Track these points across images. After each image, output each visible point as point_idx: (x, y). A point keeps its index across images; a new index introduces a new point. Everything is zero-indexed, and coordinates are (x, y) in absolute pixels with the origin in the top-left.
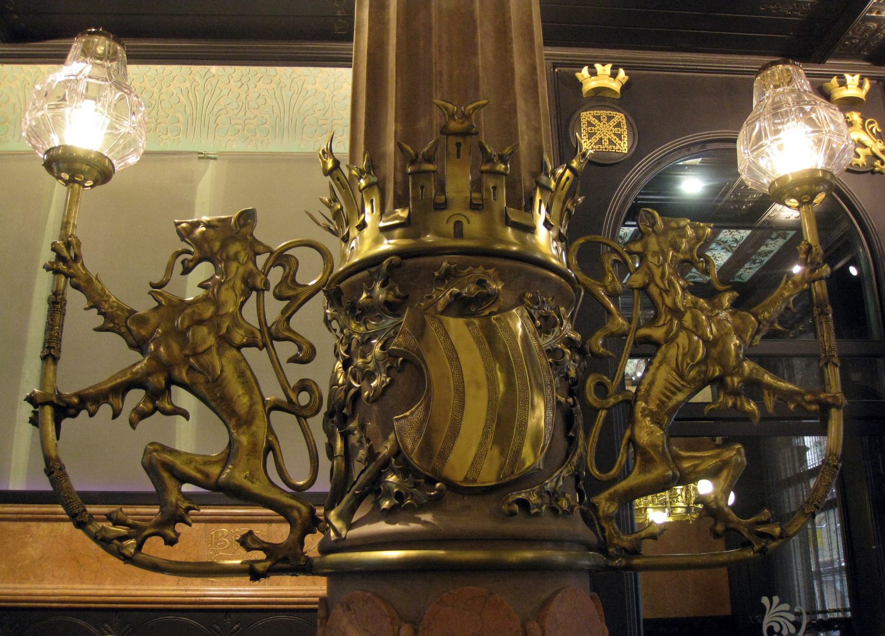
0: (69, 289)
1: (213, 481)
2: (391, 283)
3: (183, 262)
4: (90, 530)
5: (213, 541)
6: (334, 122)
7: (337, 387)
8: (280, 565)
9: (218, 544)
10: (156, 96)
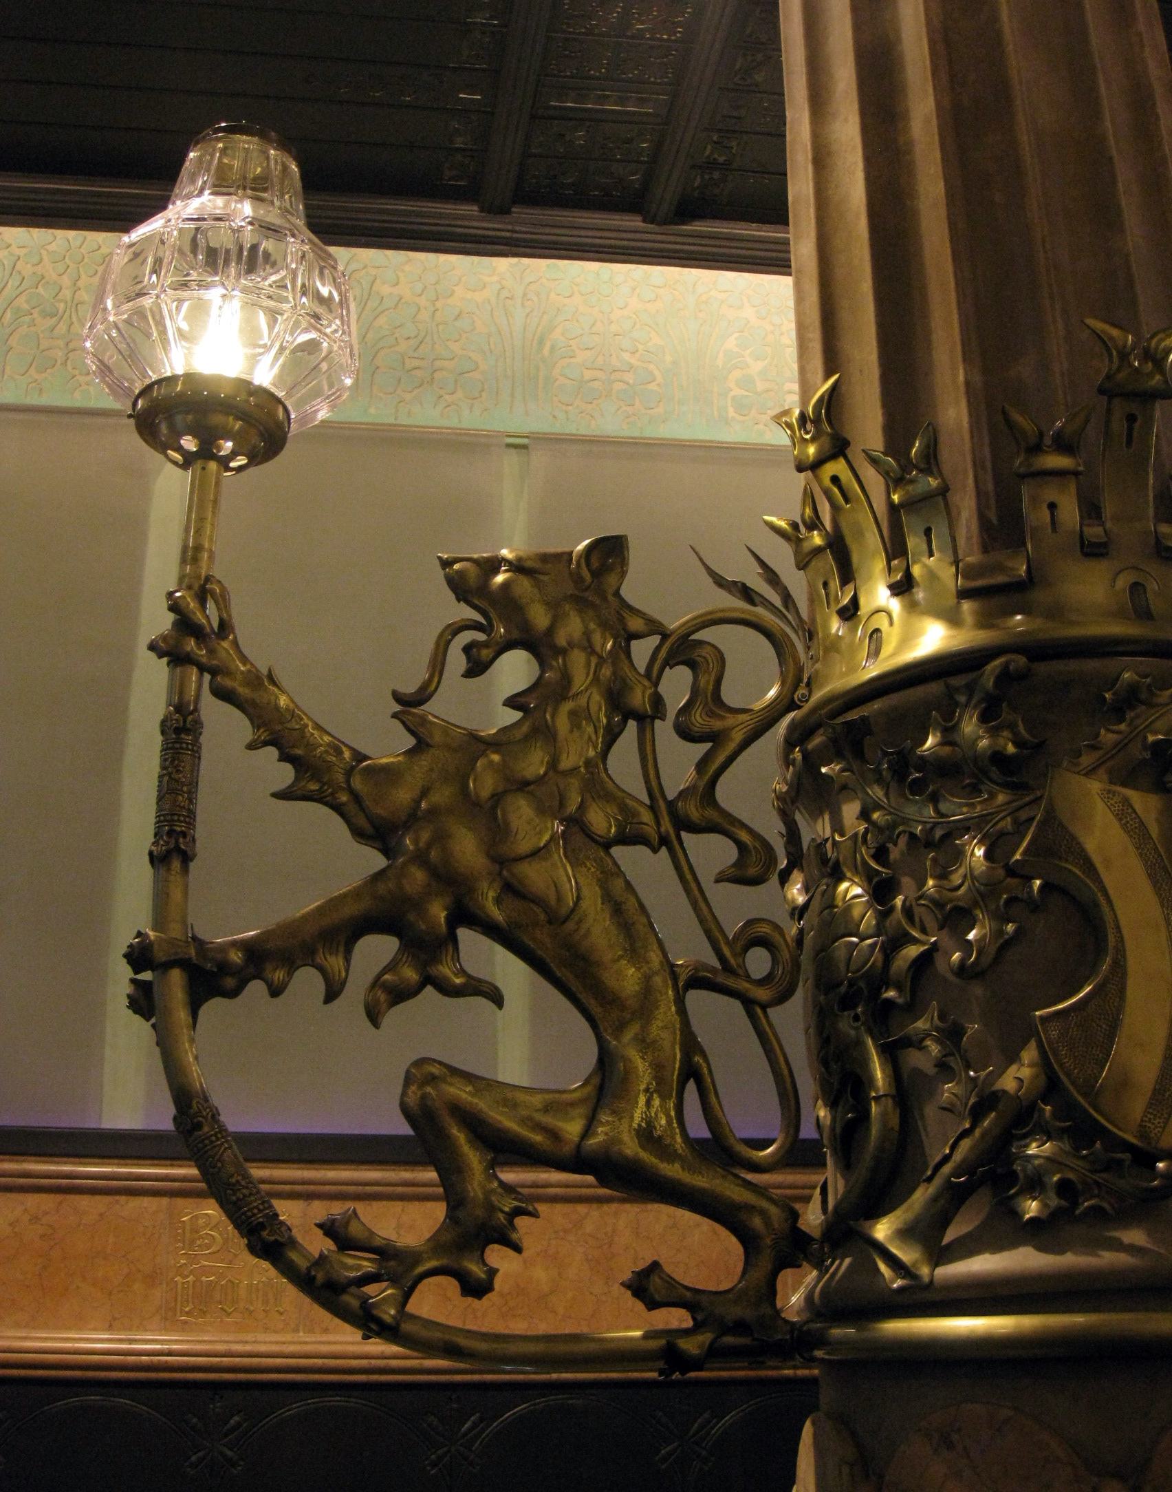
0: (207, 699)
1: (567, 1150)
2: (1006, 714)
3: (467, 649)
4: (292, 1261)
5: (188, 1235)
6: (438, 364)
7: (855, 939)
8: (729, 1340)
9: (198, 1242)
10: (67, 293)
